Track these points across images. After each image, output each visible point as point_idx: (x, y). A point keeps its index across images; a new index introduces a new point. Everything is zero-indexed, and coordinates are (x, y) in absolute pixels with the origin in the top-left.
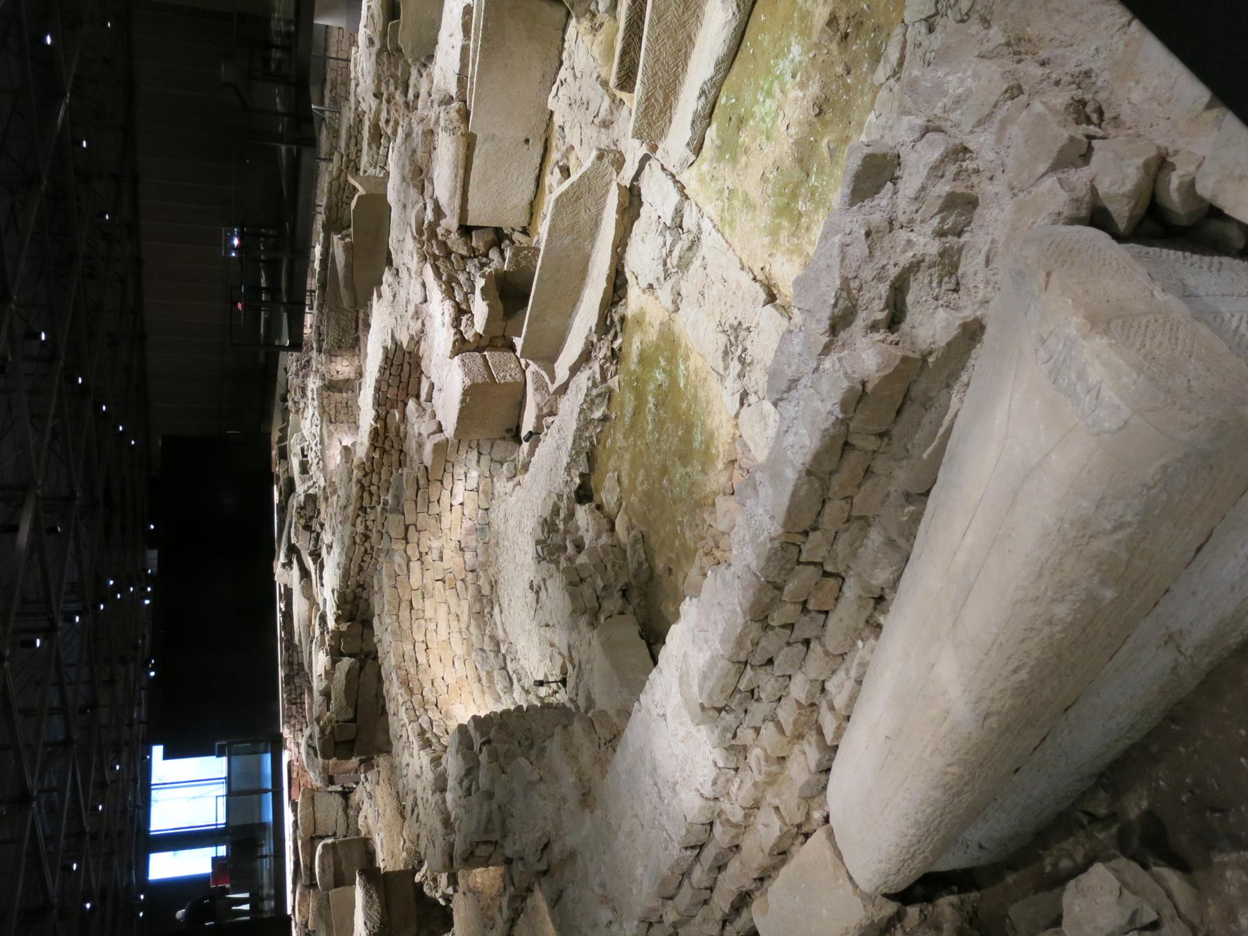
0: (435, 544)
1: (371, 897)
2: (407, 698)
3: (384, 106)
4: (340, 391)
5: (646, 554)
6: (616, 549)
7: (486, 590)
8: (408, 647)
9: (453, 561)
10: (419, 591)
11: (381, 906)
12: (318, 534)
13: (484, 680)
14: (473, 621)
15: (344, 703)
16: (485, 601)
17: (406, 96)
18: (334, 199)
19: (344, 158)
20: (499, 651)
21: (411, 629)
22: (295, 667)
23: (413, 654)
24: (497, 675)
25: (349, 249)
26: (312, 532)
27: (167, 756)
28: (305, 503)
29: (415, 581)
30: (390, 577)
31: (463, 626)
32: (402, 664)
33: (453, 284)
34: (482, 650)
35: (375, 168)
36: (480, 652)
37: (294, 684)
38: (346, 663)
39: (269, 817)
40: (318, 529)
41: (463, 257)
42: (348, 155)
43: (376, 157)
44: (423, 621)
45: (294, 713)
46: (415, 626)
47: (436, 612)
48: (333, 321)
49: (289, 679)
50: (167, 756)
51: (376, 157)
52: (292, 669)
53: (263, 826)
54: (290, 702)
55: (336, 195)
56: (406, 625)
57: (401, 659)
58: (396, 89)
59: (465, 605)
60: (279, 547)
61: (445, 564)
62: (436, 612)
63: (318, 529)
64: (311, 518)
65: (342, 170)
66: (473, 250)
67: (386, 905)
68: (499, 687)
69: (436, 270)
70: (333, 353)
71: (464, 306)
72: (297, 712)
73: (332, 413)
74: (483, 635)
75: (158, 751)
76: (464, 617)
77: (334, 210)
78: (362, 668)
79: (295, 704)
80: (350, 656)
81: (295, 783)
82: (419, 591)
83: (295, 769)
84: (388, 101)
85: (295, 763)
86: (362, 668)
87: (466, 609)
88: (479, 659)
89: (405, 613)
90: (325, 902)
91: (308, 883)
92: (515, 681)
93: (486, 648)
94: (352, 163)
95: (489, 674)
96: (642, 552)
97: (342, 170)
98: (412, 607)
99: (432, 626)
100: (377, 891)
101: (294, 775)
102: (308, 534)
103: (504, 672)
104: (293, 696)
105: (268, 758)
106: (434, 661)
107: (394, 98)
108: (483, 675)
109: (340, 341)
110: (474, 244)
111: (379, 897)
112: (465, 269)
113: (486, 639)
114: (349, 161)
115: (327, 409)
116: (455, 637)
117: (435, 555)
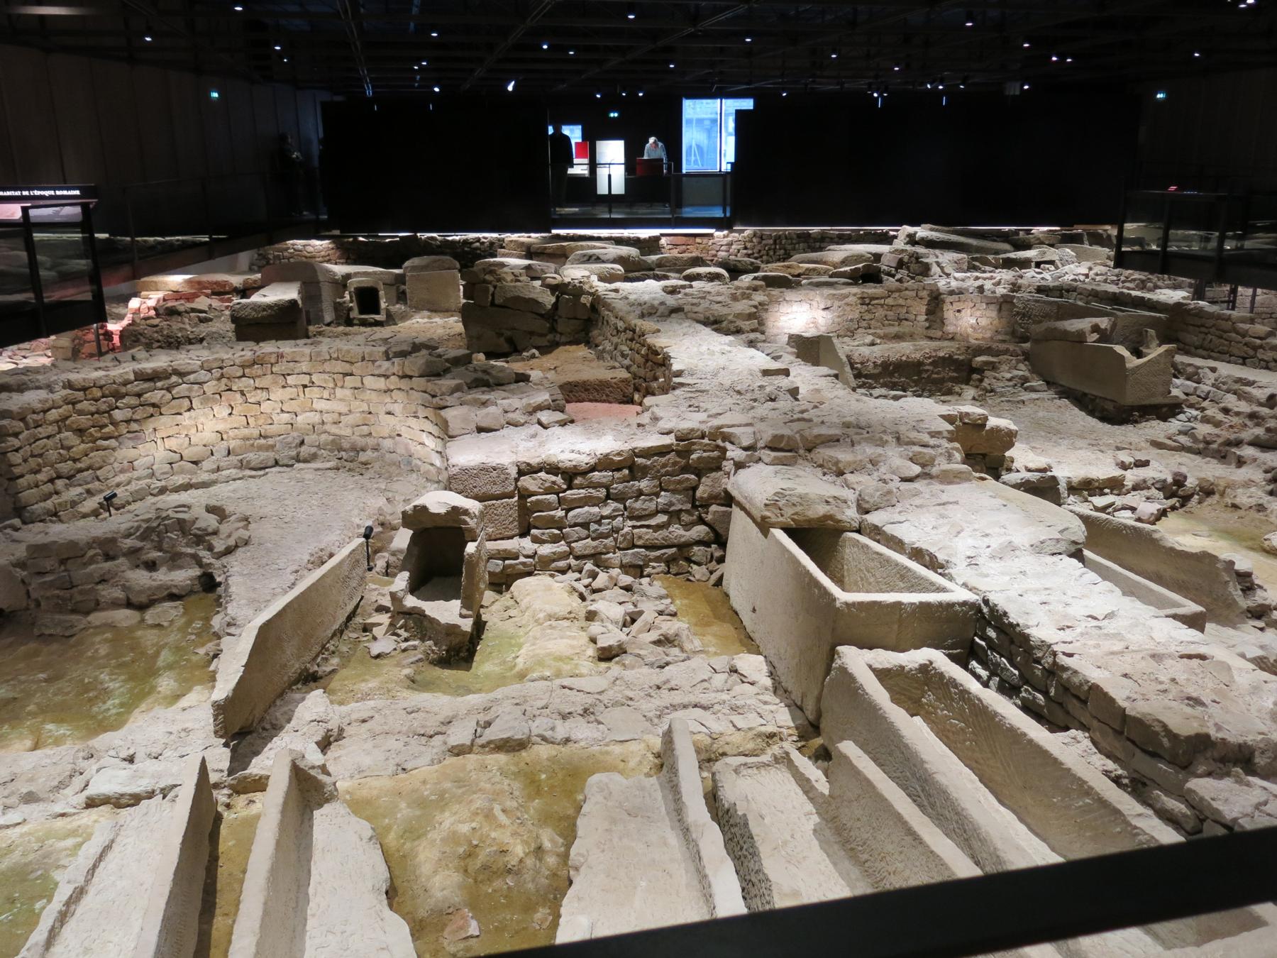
0: (397, 408)
1: (264, 310)
2: (237, 362)
3: (1244, 407)
4: (929, 313)
5: (51, 635)
6: (92, 604)
7: (363, 457)
8: (304, 367)
9: (386, 424)
10: (360, 385)
11: (254, 319)
12: (893, 276)
13: (262, 441)
14: (331, 438)
15: (508, 295)
16: (352, 454)
17: (1252, 444)
18: (1210, 322)
19: (1258, 341)
20: (298, 461)
21: (324, 372)
22: (818, 245)
23: (296, 371)
24: (269, 456)
25: (1080, 337)
26: (897, 269)
27: (740, 115)
28: (921, 262)
29: (369, 381)
30: (371, 354)
31: (326, 427)
32: (285, 360)
33: (626, 472)
34: (302, 443)
35: (1213, 385)
36: (298, 441)
37: (799, 243)
38: (548, 299)
39: (688, 212)
40: (898, 276)
41: (694, 489)
42: (1261, 347)
43: (1225, 387)
44: (331, 385)
45: (764, 242)
46: (326, 376)
47: (341, 400)
48: (1048, 309)
49: (805, 237)
50: (740, 115)
51: (1225, 387)
52: (816, 240)
53: (679, 205)
54: (777, 239)
55: (1214, 325)
56: (327, 367)
57: (289, 359)
58: (1268, 430)
59: (348, 432)
60: (948, 232)
61: (383, 417)
62: (341, 400)
63: (898, 276)
64: (908, 269)
65: (1244, 336)
66: (706, 506)
67: (257, 324)
68: (251, 456)
69: (662, 451)
70: (1005, 307)
71: (578, 481)
72: (766, 245)
73: (890, 301)
74: (319, 447)
75: (748, 104)
76: (334, 429)
77: (1199, 322)
78: (542, 316)
79: (775, 243)
80: (555, 306)
81: (691, 240)
82: (360, 385)
83: (705, 240)
84: (1252, 416)
85: (711, 241)
86: (542, 316)
87: (343, 433)
88: (290, 439)
89: (340, 367)
90: (447, 266)
91: (532, 250)
92: (253, 473)
93: (303, 448)
94: (1251, 352)
95: (273, 447)
96: (52, 631)
97: (1244, 336)
98: (346, 375)
99: (326, 395)
100: (270, 316)
101: (698, 240)
102: (894, 265)
103: (271, 462)
104: (783, 242)
105: (718, 213)
106: (290, 392)
107: (1258, 425)
108: (271, 441)
109: (1029, 318)
110: (714, 508)
111: (262, 317)
112: (662, 489)
113: (313, 450)
114: (1255, 348)
115: (896, 295)
116: (315, 418)
117: (391, 407)
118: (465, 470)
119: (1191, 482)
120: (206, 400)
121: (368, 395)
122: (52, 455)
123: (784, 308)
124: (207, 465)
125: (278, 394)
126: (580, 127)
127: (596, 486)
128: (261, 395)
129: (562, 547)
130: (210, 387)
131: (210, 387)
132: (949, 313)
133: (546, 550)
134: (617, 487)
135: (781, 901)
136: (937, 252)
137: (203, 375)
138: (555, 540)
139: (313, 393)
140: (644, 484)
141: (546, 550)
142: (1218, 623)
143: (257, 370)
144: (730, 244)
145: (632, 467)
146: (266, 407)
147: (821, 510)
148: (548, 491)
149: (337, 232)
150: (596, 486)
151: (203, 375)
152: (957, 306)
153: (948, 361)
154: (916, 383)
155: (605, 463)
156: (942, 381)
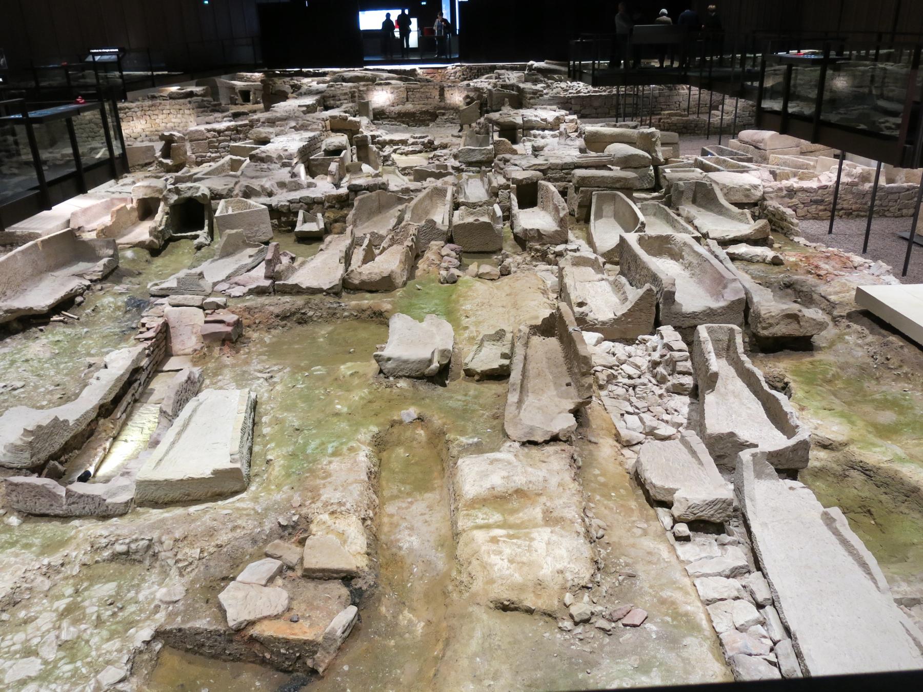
81: (435, 71)
89: (178, 107)
106: (164, 116)
118: (191, 131)
119: (436, 143)
120: (138, 118)
121: (186, 116)
122: (87, 130)
123: (375, 93)
124: (139, 139)
125: (161, 116)
126: (360, 13)
127: (227, 136)
128: (155, 117)
129: (218, 154)
130: (139, 113)
131: (139, 113)
132: (447, 95)
133: (213, 155)
134: (233, 136)
135: (814, 674)
136: (509, 72)
137: (136, 109)
138: (216, 152)
139: (171, 116)
140: (241, 136)
141: (213, 155)
142: (133, 90)
143: (153, 108)
144: (456, 73)
145: (237, 131)
146: (157, 121)
147: (264, 135)
148: (214, 137)
149: (266, 69)
150: (227, 136)
151: (136, 109)
152: (451, 92)
153: (427, 112)
154: (413, 121)
155: (228, 129)
156: (425, 120)
